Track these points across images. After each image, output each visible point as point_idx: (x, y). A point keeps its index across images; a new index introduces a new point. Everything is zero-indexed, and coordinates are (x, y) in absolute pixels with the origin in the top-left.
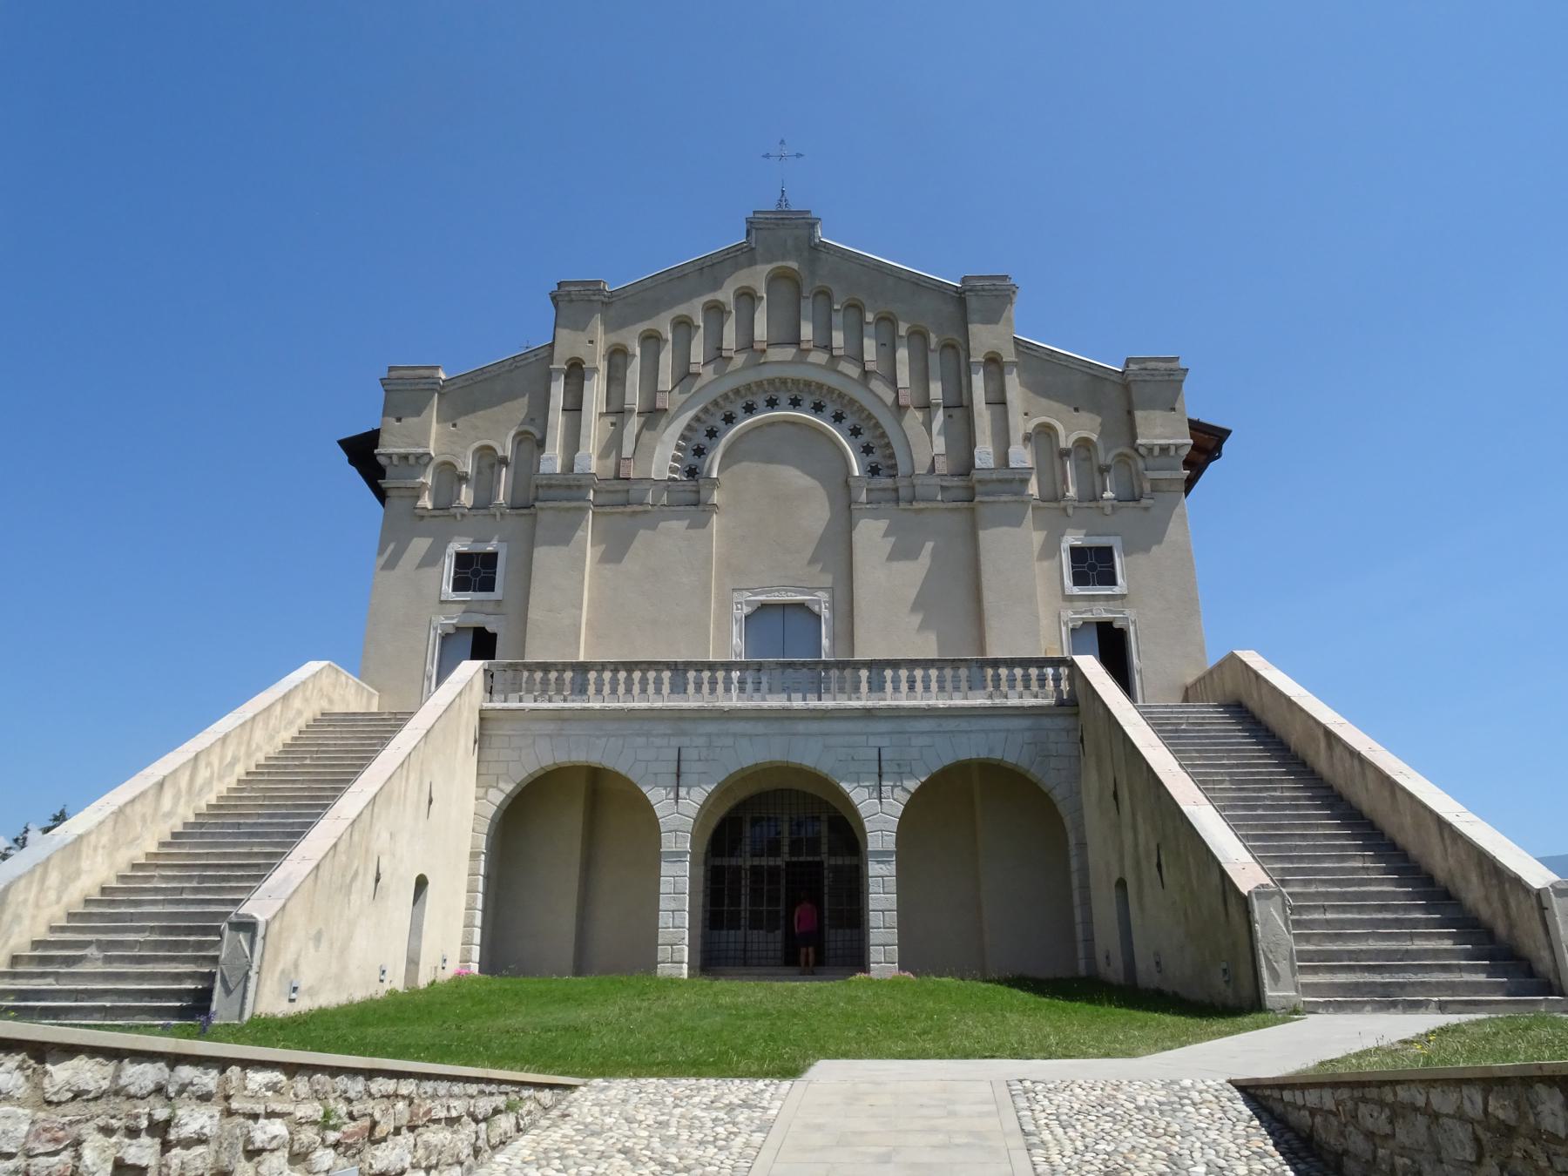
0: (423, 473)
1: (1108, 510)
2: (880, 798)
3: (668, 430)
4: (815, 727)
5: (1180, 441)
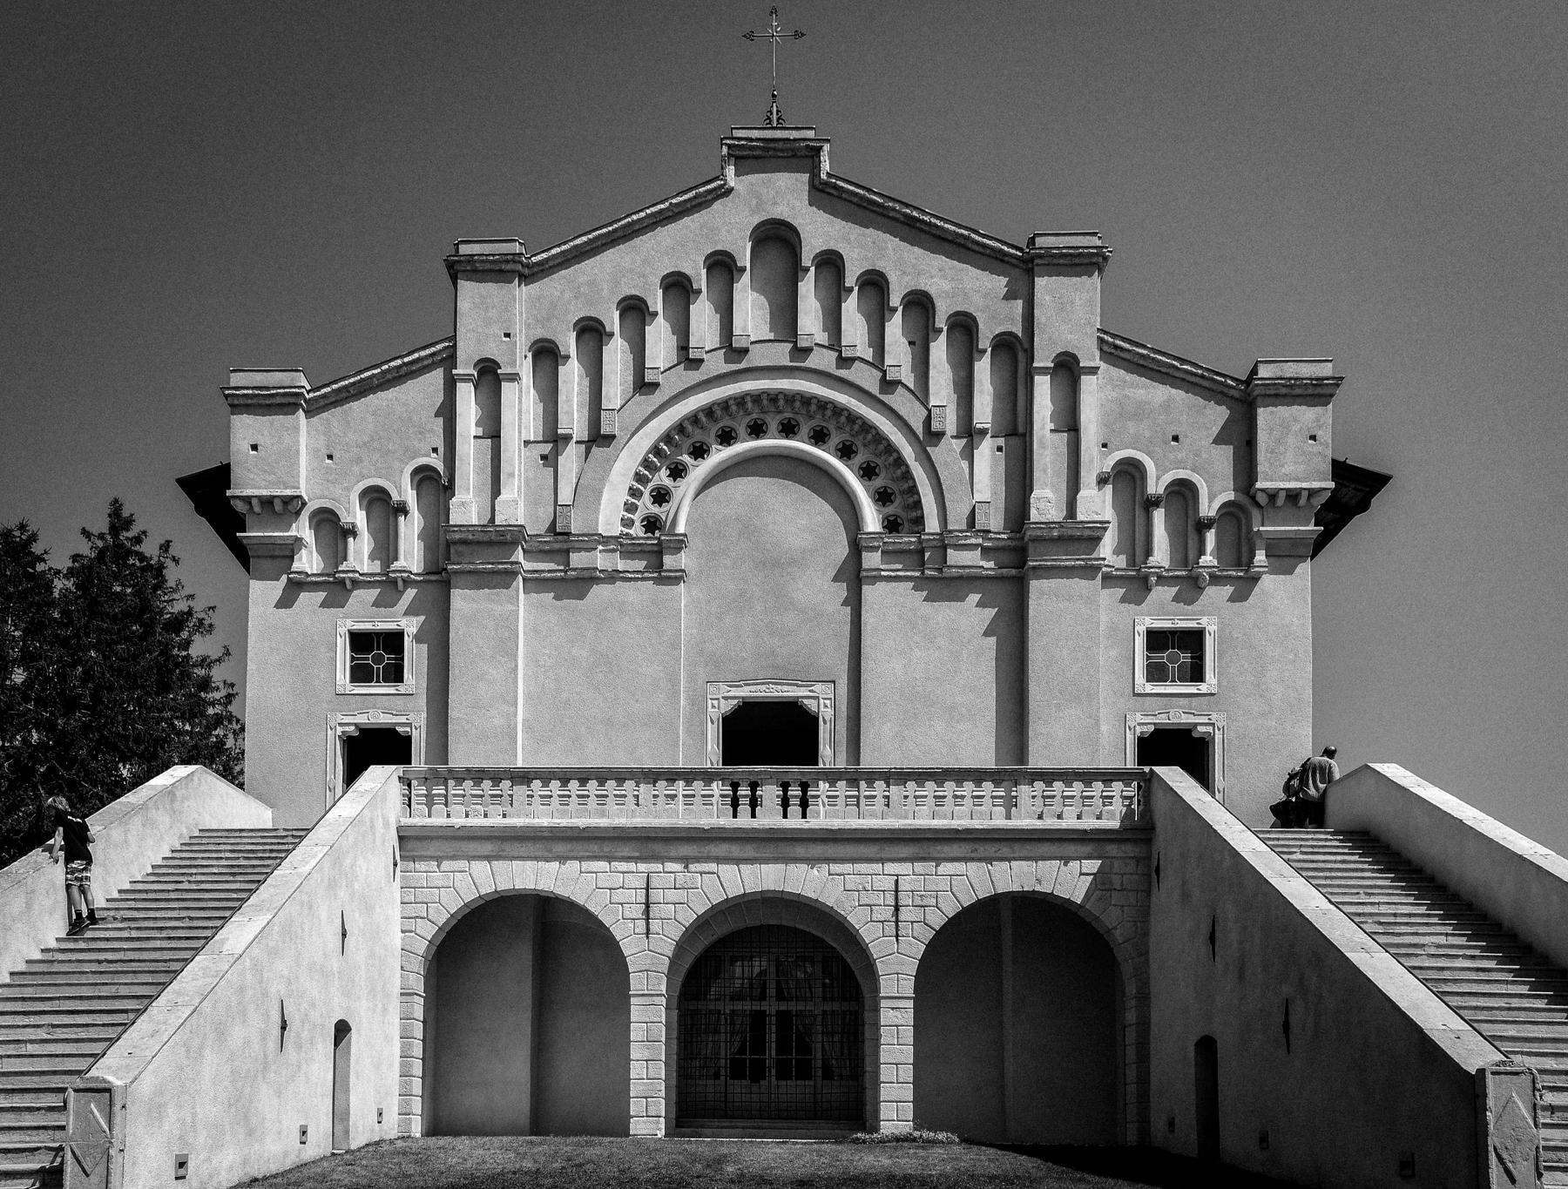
5: (1316, 485)
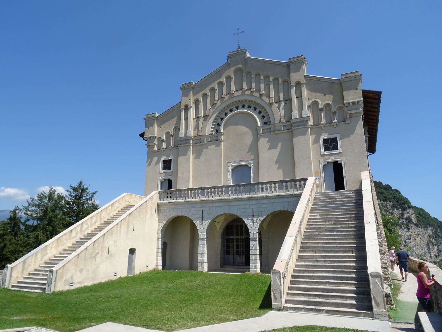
0: (154, 141)
1: (335, 126)
2: (253, 223)
3: (210, 120)
4: (236, 203)
